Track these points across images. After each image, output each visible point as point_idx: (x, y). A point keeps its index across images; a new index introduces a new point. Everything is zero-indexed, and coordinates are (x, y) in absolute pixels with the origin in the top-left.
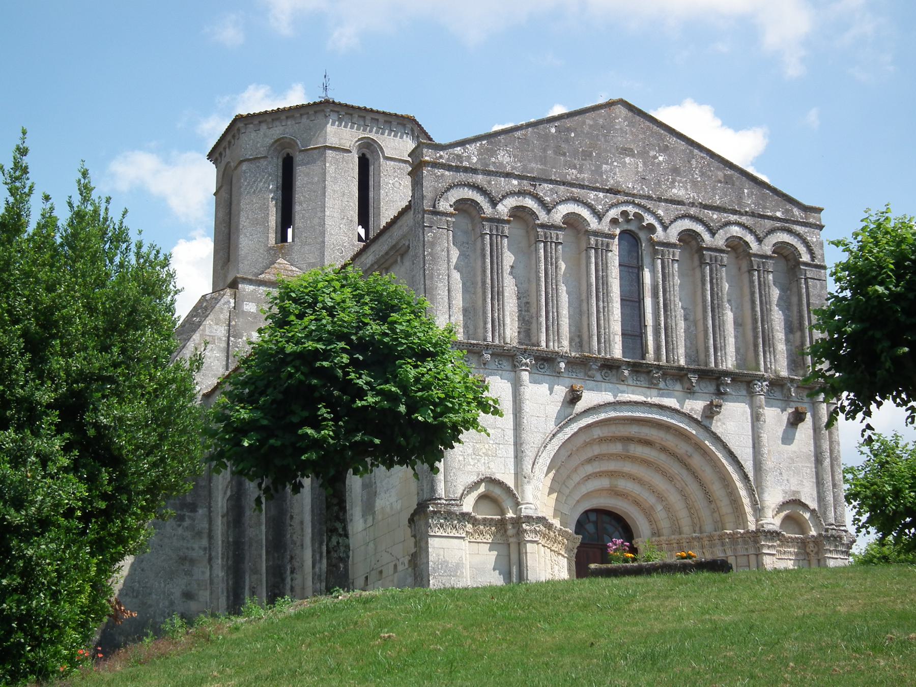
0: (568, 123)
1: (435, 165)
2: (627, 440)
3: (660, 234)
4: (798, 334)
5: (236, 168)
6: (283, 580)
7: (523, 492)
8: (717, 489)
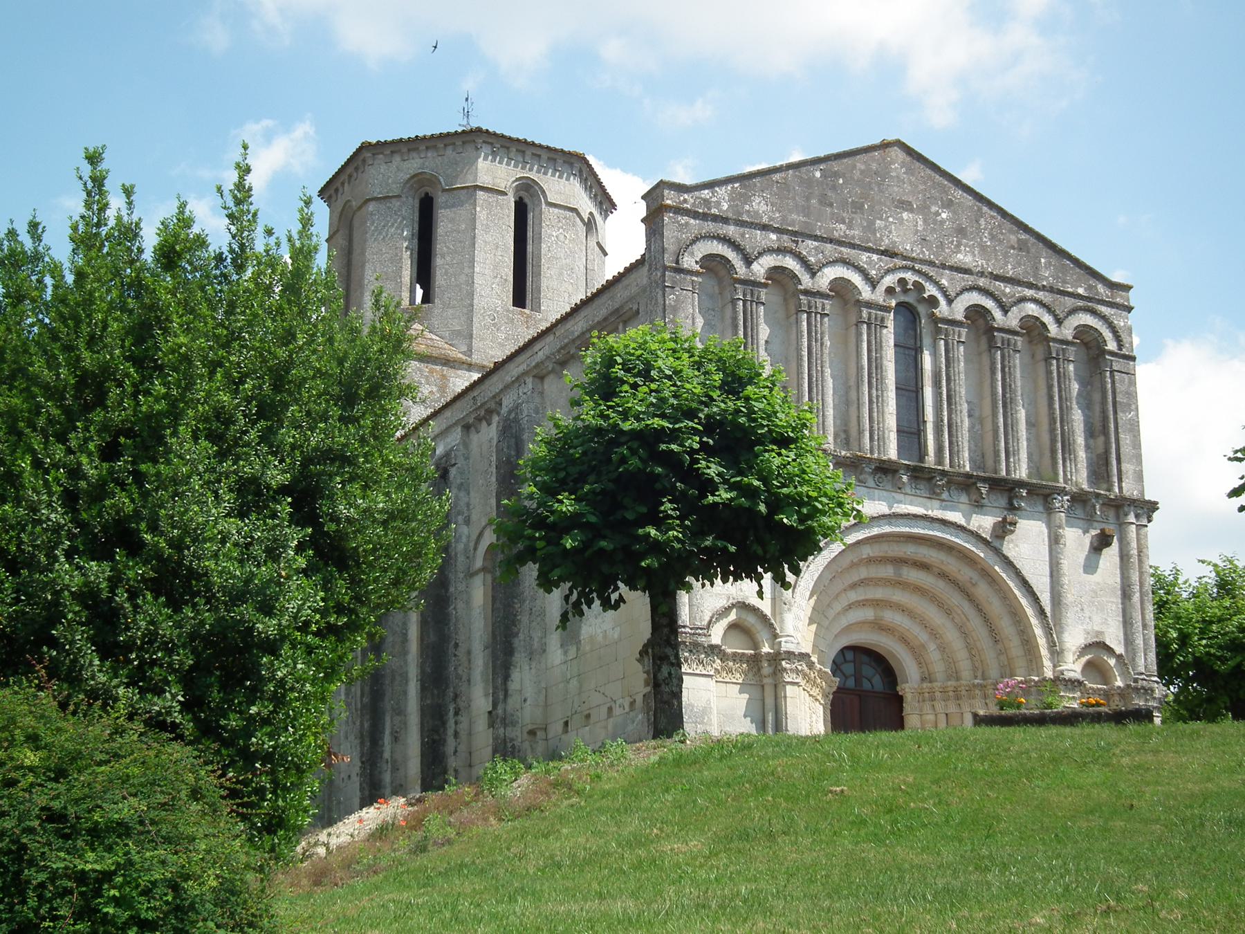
0: (836, 166)
1: (678, 210)
2: (899, 562)
3: (943, 309)
4: (1101, 439)
5: (360, 208)
6: (444, 723)
7: (782, 621)
8: (1006, 626)
